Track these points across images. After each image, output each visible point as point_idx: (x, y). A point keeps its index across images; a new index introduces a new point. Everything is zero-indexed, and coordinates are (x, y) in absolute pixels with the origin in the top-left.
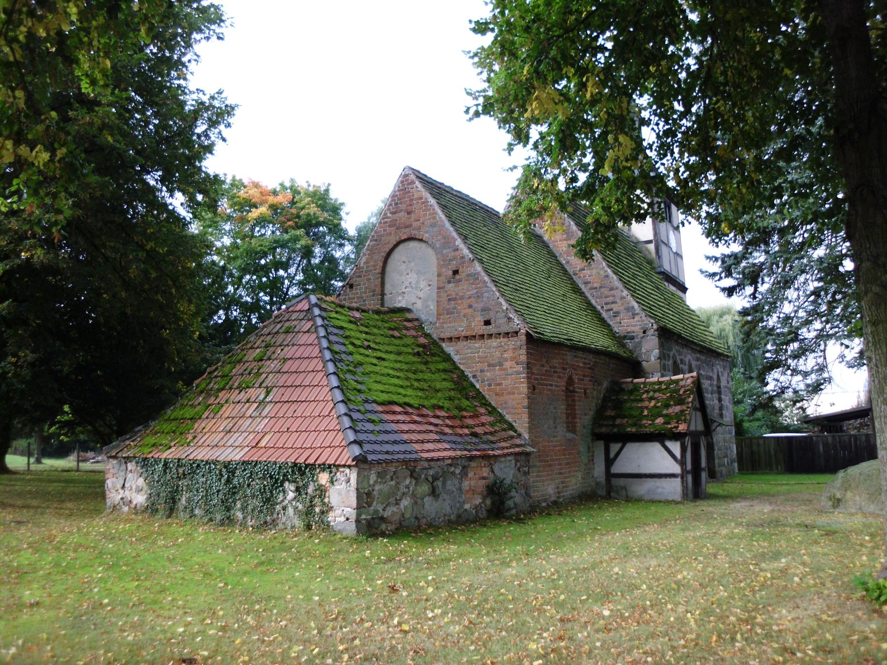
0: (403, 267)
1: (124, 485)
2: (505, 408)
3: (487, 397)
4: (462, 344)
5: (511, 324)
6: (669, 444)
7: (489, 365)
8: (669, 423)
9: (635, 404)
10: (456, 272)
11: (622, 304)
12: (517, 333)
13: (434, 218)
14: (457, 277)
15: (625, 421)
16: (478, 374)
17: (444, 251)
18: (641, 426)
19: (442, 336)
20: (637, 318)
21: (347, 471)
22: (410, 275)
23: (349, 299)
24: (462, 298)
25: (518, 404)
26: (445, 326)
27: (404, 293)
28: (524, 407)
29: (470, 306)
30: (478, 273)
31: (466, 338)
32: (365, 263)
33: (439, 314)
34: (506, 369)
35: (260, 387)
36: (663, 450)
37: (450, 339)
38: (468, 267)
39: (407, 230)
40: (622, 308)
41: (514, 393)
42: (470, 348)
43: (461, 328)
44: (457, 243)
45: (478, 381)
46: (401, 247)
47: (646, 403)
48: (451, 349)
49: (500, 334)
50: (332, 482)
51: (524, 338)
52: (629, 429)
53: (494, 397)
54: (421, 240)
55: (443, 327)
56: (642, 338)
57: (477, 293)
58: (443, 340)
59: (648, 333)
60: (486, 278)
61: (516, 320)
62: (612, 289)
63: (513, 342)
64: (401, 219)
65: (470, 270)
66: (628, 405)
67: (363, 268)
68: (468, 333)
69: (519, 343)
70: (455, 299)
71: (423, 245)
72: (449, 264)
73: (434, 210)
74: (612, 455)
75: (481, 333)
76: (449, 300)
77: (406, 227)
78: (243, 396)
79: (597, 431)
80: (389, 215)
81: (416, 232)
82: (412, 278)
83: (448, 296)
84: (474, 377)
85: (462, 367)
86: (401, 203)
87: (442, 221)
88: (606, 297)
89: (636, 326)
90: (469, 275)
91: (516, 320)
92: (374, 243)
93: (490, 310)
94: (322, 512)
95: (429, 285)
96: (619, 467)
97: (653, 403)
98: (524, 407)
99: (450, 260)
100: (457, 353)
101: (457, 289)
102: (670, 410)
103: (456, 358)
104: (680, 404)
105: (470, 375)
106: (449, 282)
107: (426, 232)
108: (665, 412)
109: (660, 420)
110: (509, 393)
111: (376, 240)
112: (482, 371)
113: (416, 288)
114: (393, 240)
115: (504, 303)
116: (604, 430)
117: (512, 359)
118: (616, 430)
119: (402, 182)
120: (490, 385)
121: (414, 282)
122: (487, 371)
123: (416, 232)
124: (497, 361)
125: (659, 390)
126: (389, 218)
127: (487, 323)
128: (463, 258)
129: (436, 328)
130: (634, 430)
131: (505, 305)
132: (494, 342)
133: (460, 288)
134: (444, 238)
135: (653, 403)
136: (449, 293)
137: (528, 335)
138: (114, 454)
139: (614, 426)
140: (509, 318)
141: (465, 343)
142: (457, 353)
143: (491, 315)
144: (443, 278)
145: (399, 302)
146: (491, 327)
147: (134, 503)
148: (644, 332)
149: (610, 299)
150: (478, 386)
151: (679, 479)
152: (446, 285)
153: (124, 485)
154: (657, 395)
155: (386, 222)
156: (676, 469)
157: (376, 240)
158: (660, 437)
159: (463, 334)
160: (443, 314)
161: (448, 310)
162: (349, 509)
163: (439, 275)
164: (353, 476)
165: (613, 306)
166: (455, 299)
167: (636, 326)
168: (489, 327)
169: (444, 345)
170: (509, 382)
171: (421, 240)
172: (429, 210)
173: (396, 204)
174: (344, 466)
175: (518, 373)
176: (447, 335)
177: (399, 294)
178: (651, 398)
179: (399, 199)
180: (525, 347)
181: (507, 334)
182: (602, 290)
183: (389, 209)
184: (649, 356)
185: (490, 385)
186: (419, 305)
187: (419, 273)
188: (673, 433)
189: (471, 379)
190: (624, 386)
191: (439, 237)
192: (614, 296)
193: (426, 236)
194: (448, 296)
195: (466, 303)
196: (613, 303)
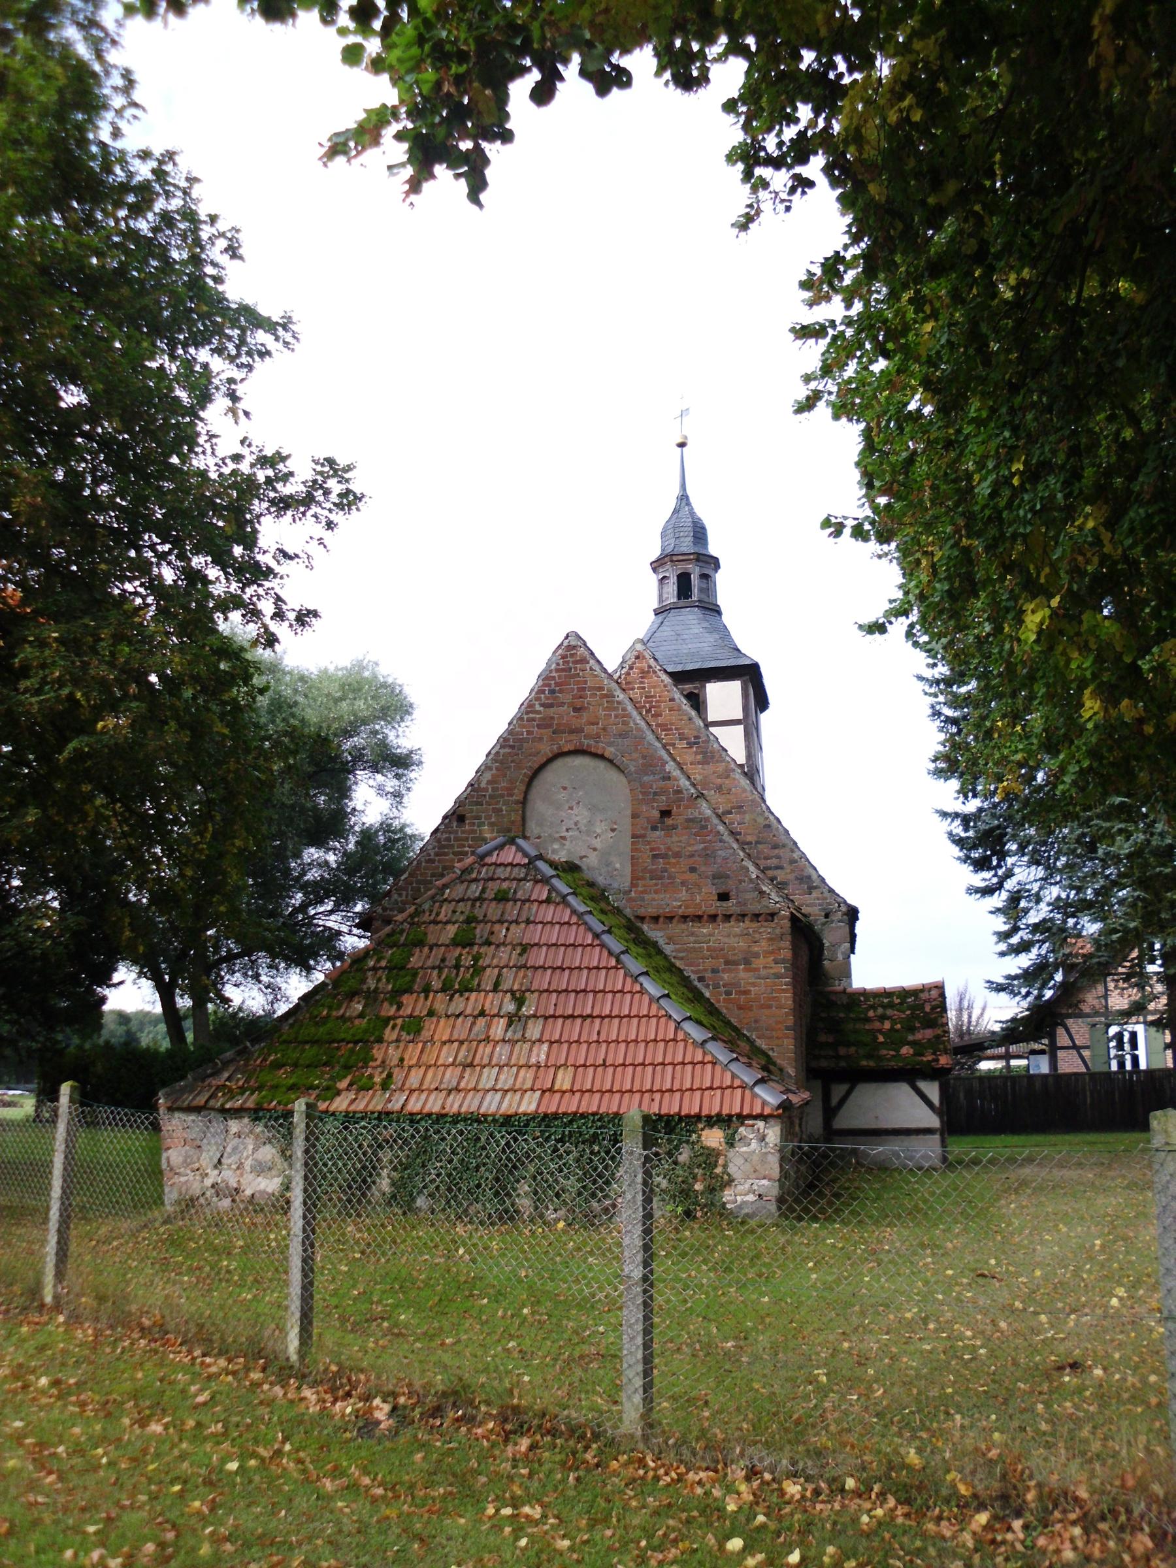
0: (562, 796)
1: (219, 1162)
2: (756, 1029)
3: (724, 1011)
4: (676, 928)
5: (764, 902)
6: (923, 1085)
7: (727, 963)
8: (923, 1055)
9: (859, 1026)
10: (666, 813)
11: (792, 871)
12: (772, 915)
13: (625, 723)
14: (669, 821)
15: (852, 1050)
16: (708, 975)
17: (646, 778)
18: (880, 1058)
19: (641, 912)
20: (815, 894)
21: (761, 1124)
22: (575, 811)
23: (456, 839)
24: (677, 855)
25: (778, 1022)
26: (647, 897)
27: (563, 838)
28: (788, 1028)
29: (693, 870)
30: (707, 819)
31: (685, 918)
32: (489, 782)
33: (635, 879)
34: (757, 970)
35: (495, 989)
36: (913, 1093)
37: (656, 919)
38: (687, 807)
39: (573, 737)
40: (791, 877)
41: (770, 1007)
42: (692, 934)
43: (677, 901)
44: (667, 768)
45: (707, 986)
46: (559, 763)
47: (877, 1025)
48: (660, 934)
49: (744, 916)
50: (731, 1144)
51: (787, 923)
52: (864, 1063)
53: (737, 1012)
54: (601, 757)
55: (643, 899)
56: (824, 924)
57: (705, 849)
58: (642, 919)
59: (832, 917)
60: (721, 828)
61: (773, 895)
62: (775, 847)
63: (767, 930)
64: (561, 717)
65: (691, 813)
66: (850, 1026)
67: (486, 790)
68: (691, 911)
69: (778, 931)
70: (664, 856)
71: (602, 765)
72: (654, 800)
73: (624, 710)
74: (834, 1101)
75: (712, 911)
76: (655, 856)
77: (572, 732)
78: (458, 1004)
79: (814, 1064)
80: (538, 708)
81: (592, 742)
82: (581, 815)
83: (652, 850)
84: (701, 979)
85: (678, 963)
86: (561, 691)
87: (639, 730)
88: (766, 858)
89: (813, 905)
90: (689, 820)
91: (773, 895)
92: (507, 750)
93: (728, 877)
94: (711, 1190)
95: (613, 830)
96: (847, 1119)
97: (887, 1025)
98: (788, 1028)
99: (655, 794)
100: (670, 940)
101: (668, 840)
102: (918, 1036)
103: (668, 949)
104: (929, 1027)
105: (693, 977)
106: (654, 828)
107: (610, 744)
108: (910, 1038)
109: (905, 1050)
110: (762, 1007)
111: (512, 747)
112: (714, 971)
113: (588, 833)
114: (546, 749)
115: (752, 868)
116: (824, 1064)
117: (768, 953)
118: (843, 1064)
119: (563, 657)
120: (728, 993)
121: (583, 822)
122: (724, 971)
123: (592, 742)
124: (741, 956)
125: (891, 1005)
126: (539, 712)
127: (724, 897)
128: (679, 792)
129: (631, 900)
130: (872, 1064)
131: (754, 873)
132: (737, 928)
133: (675, 838)
134: (644, 757)
135: (887, 1025)
136: (654, 845)
137: (794, 919)
138: (202, 1103)
139: (838, 1057)
140: (762, 893)
141: (684, 926)
142: (670, 940)
143: (731, 886)
144: (642, 821)
145: (554, 851)
146: (730, 903)
147: (248, 1192)
148: (827, 916)
149: (774, 862)
150: (707, 995)
151: (937, 1137)
152: (649, 832)
153: (219, 1162)
154: (889, 1012)
155: (533, 720)
156: (934, 1122)
157: (512, 747)
158: (910, 1075)
159: (680, 912)
160: (643, 878)
161: (651, 872)
162: (765, 1182)
163: (635, 816)
164: (773, 1134)
165: (778, 873)
166: (664, 856)
167: (813, 905)
168: (724, 904)
169: (645, 927)
170: (763, 989)
171: (611, 761)
172: (616, 709)
173: (552, 692)
174: (756, 1117)
175: (778, 976)
176: (652, 911)
177: (555, 840)
178: (882, 1018)
179: (557, 684)
180: (789, 938)
181: (756, 917)
182: (760, 846)
183: (537, 699)
184: (835, 952)
185: (728, 993)
186: (592, 860)
187: (593, 808)
188: (934, 1069)
189: (696, 983)
190: (833, 998)
191: (635, 755)
192: (778, 857)
193: (610, 751)
194: (652, 850)
195: (684, 864)
196: (777, 868)
